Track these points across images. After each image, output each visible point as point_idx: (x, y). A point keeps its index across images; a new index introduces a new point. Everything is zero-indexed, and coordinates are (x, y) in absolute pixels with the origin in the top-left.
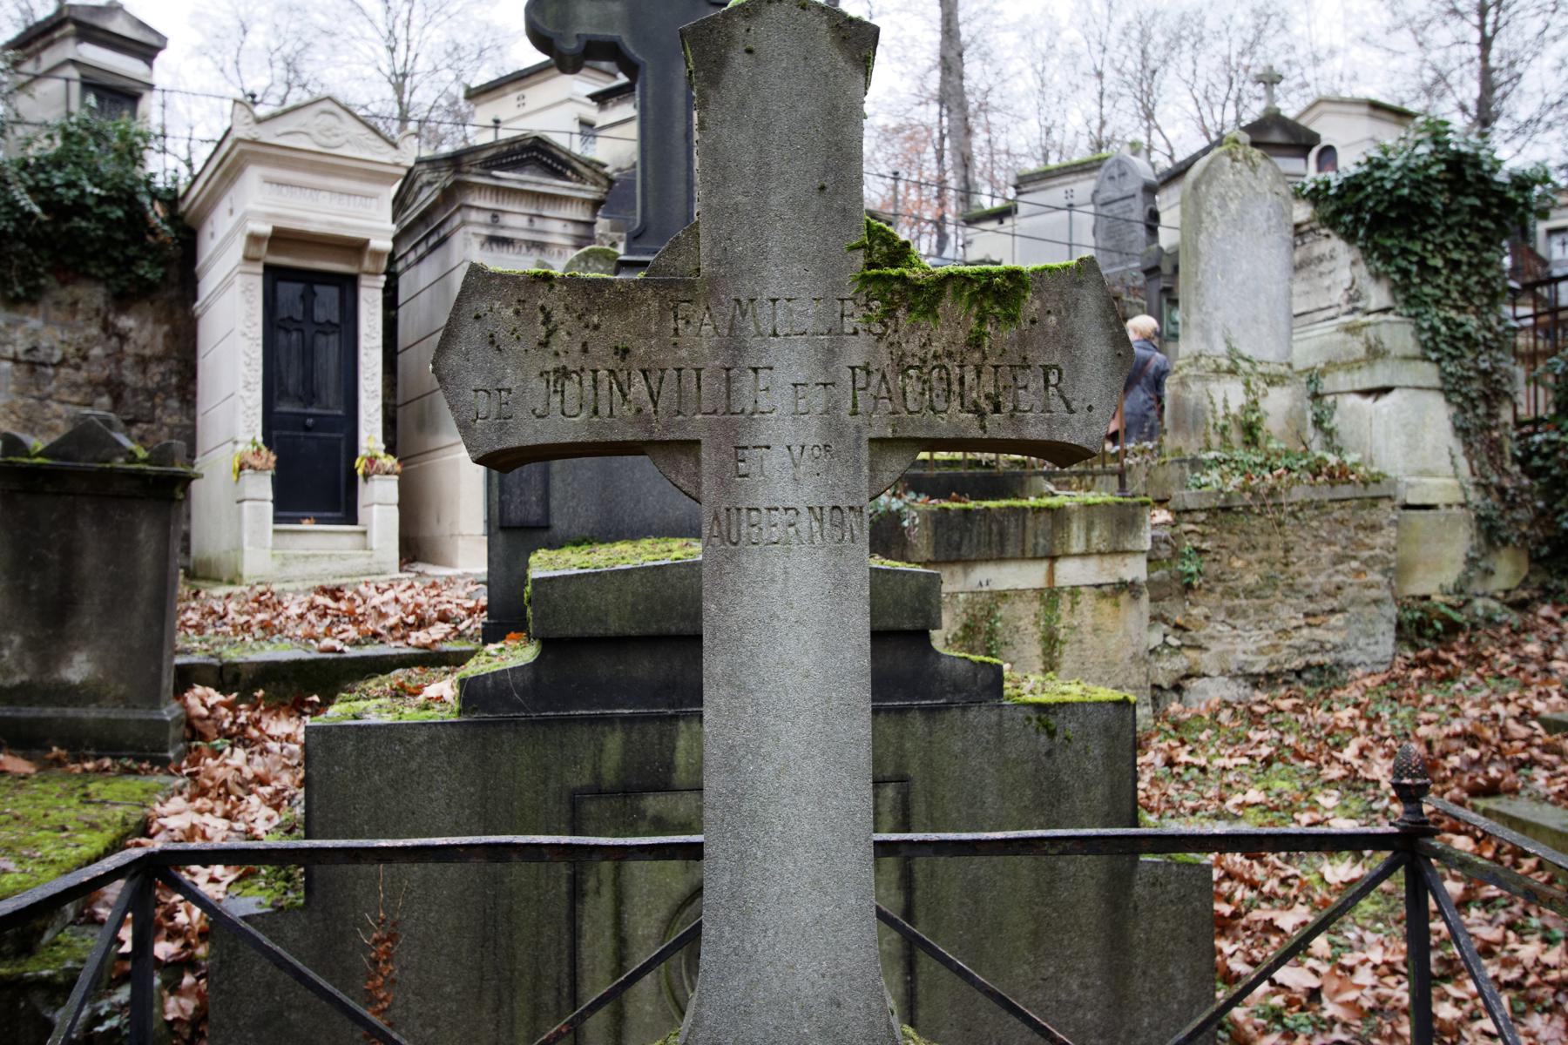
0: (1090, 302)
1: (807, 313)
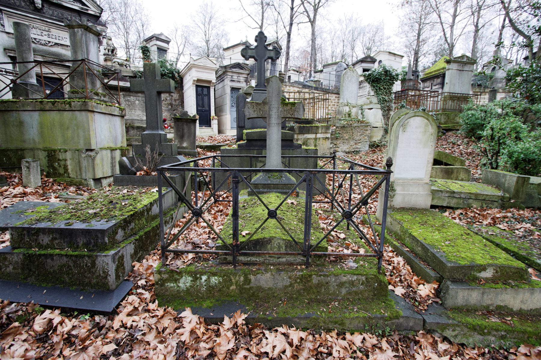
0: (301, 105)
1: (276, 106)
